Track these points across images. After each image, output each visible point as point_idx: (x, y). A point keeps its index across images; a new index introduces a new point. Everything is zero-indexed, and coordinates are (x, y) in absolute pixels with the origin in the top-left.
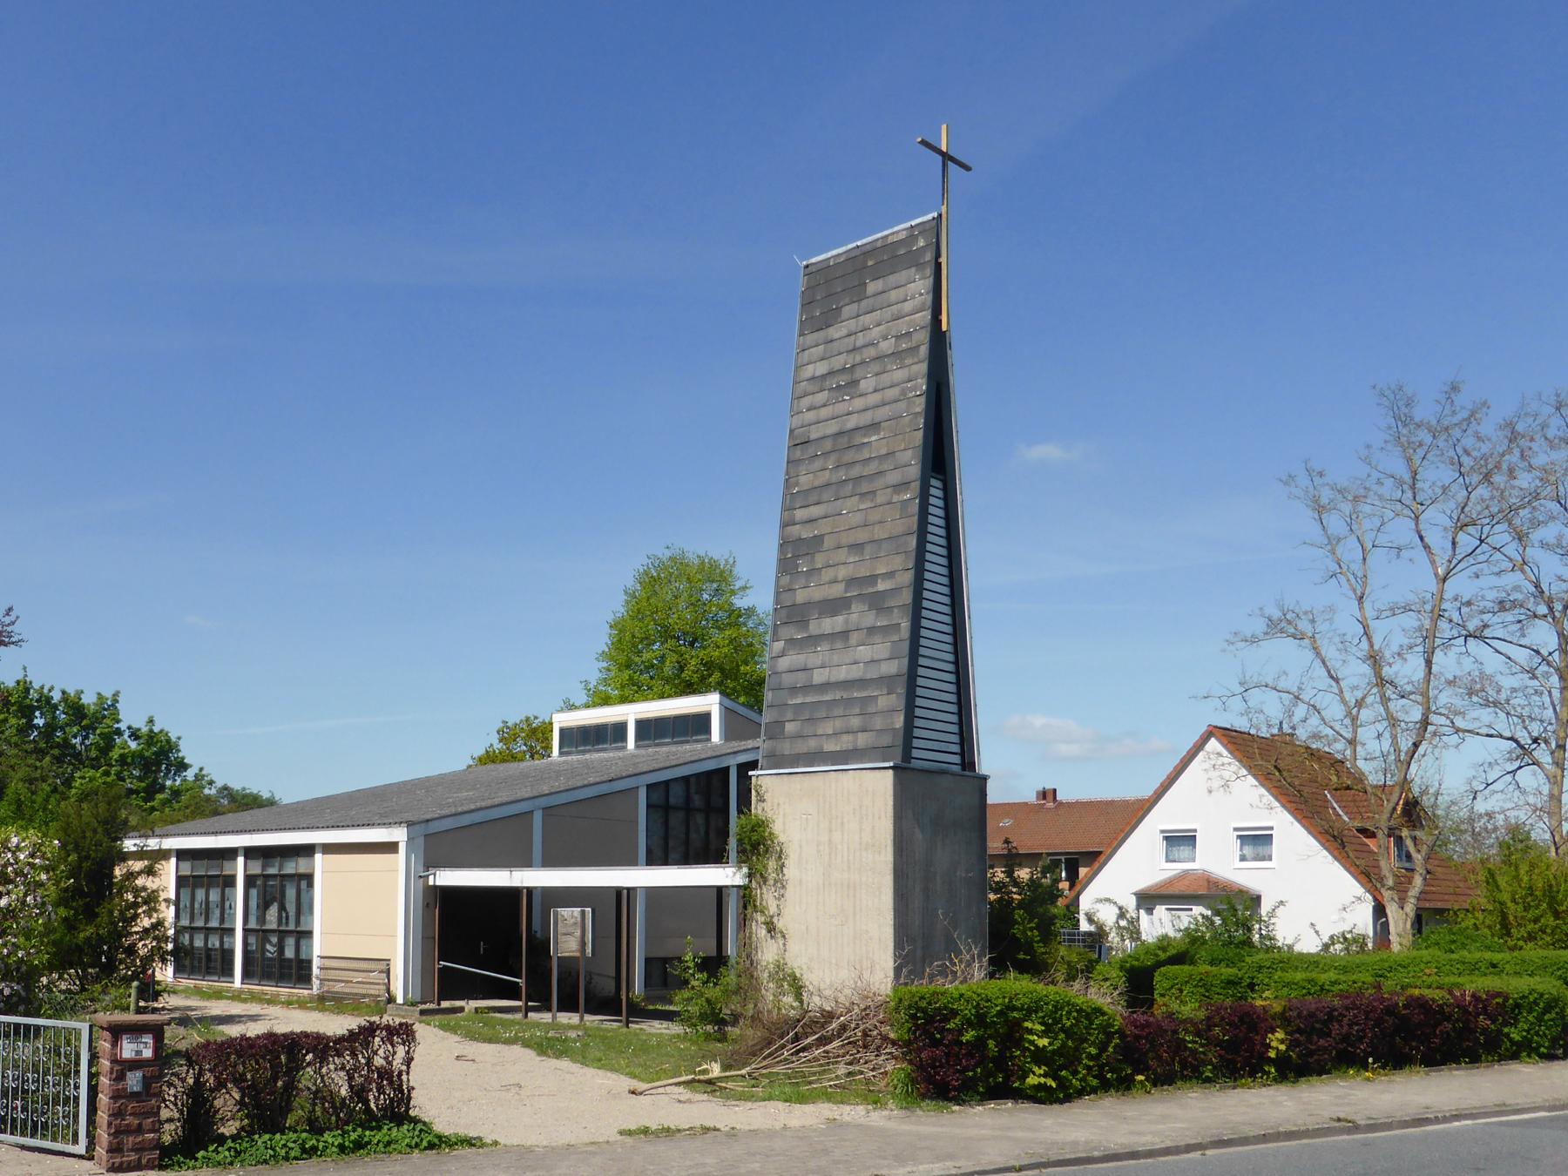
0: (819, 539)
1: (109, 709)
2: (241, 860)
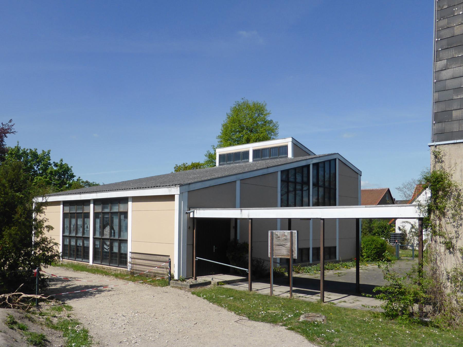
1: (46, 155)
2: (92, 205)
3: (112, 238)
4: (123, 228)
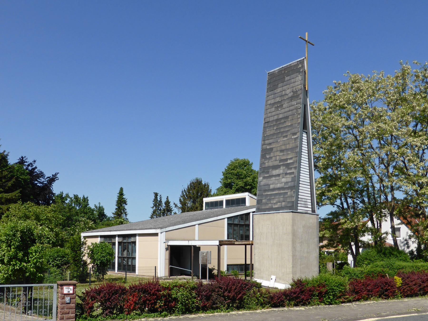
0: (271, 149)
4: (134, 250)
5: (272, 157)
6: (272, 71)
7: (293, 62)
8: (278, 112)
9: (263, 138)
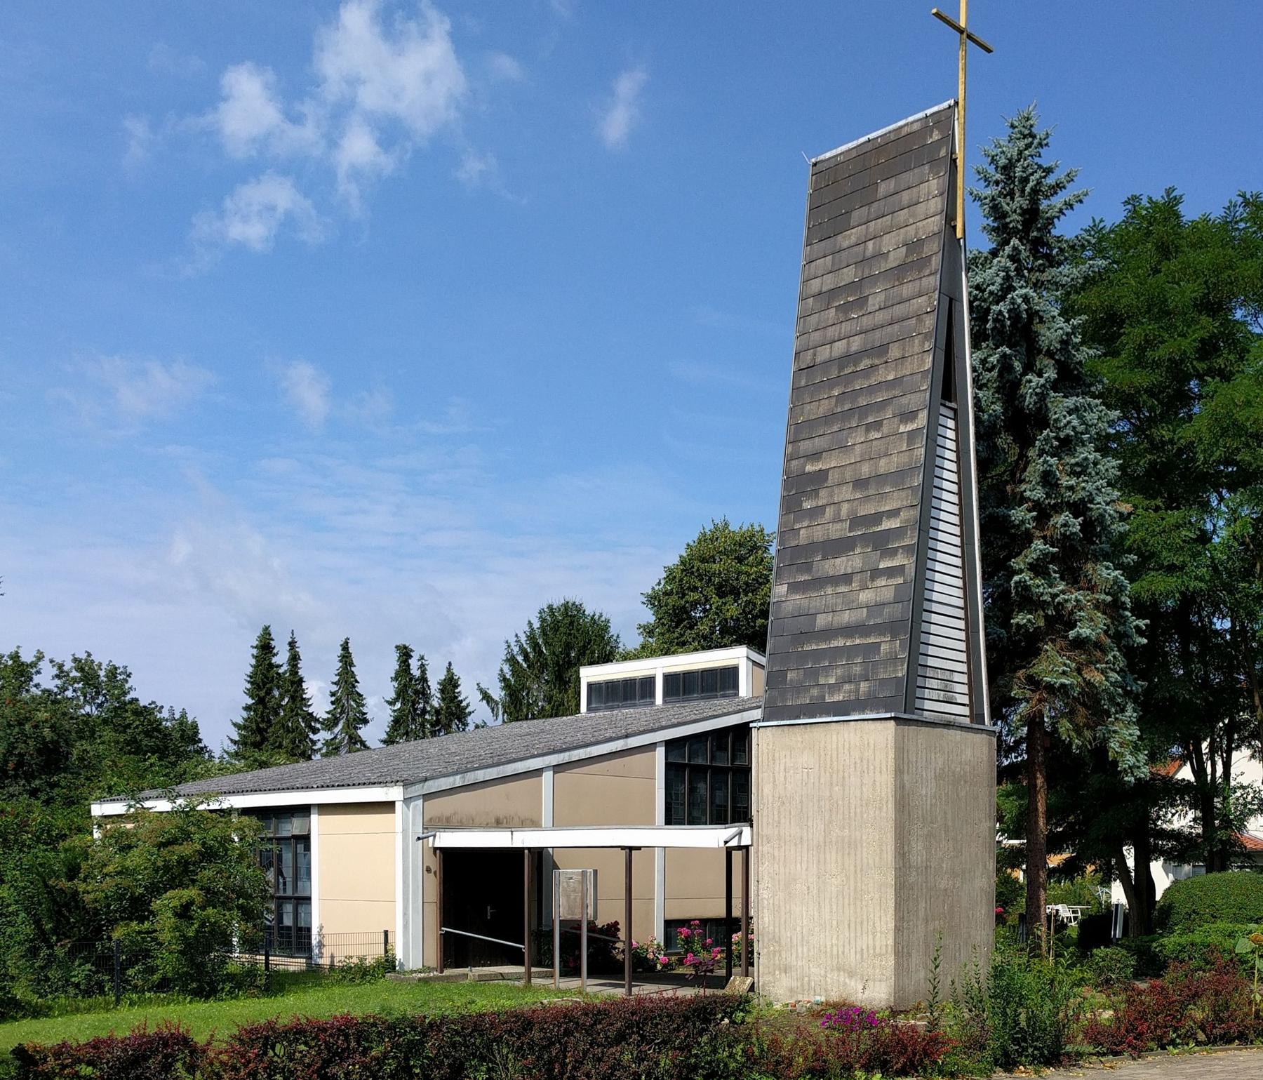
0: (823, 474)
3: (281, 894)
4: (303, 871)
5: (824, 506)
6: (828, 155)
7: (911, 119)
8: (846, 328)
9: (788, 432)
